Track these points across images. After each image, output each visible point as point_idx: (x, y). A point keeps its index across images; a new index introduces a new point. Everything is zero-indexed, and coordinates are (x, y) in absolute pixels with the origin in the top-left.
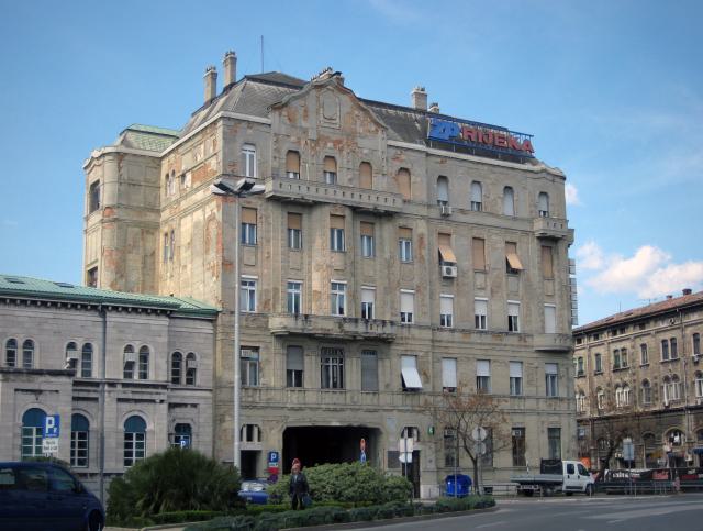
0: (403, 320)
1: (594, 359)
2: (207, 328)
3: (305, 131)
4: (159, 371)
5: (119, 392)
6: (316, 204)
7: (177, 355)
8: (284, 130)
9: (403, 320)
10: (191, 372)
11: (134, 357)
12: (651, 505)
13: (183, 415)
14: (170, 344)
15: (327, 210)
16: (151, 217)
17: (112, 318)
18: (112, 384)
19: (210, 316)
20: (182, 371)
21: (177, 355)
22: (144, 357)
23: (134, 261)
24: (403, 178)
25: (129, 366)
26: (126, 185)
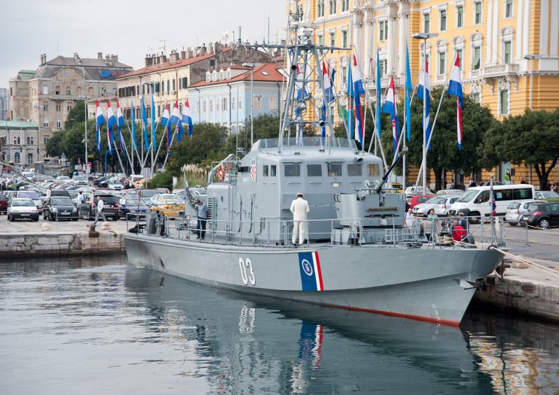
0: (177, 58)
1: (423, 18)
2: (36, 131)
3: (61, 80)
4: (23, 142)
5: (13, 147)
6: (63, 100)
7: (28, 138)
8: (55, 81)
9: (177, 58)
10: (32, 142)
11: (16, 139)
12: (231, 195)
13: (30, 152)
14: (26, 135)
15: (67, 101)
16: (26, 98)
17: (11, 131)
18: (11, 145)
19: (37, 128)
20: (30, 141)
21: (28, 138)
22: (19, 139)
23: (22, 110)
24: (91, 90)
25: (15, 141)
26: (19, 90)
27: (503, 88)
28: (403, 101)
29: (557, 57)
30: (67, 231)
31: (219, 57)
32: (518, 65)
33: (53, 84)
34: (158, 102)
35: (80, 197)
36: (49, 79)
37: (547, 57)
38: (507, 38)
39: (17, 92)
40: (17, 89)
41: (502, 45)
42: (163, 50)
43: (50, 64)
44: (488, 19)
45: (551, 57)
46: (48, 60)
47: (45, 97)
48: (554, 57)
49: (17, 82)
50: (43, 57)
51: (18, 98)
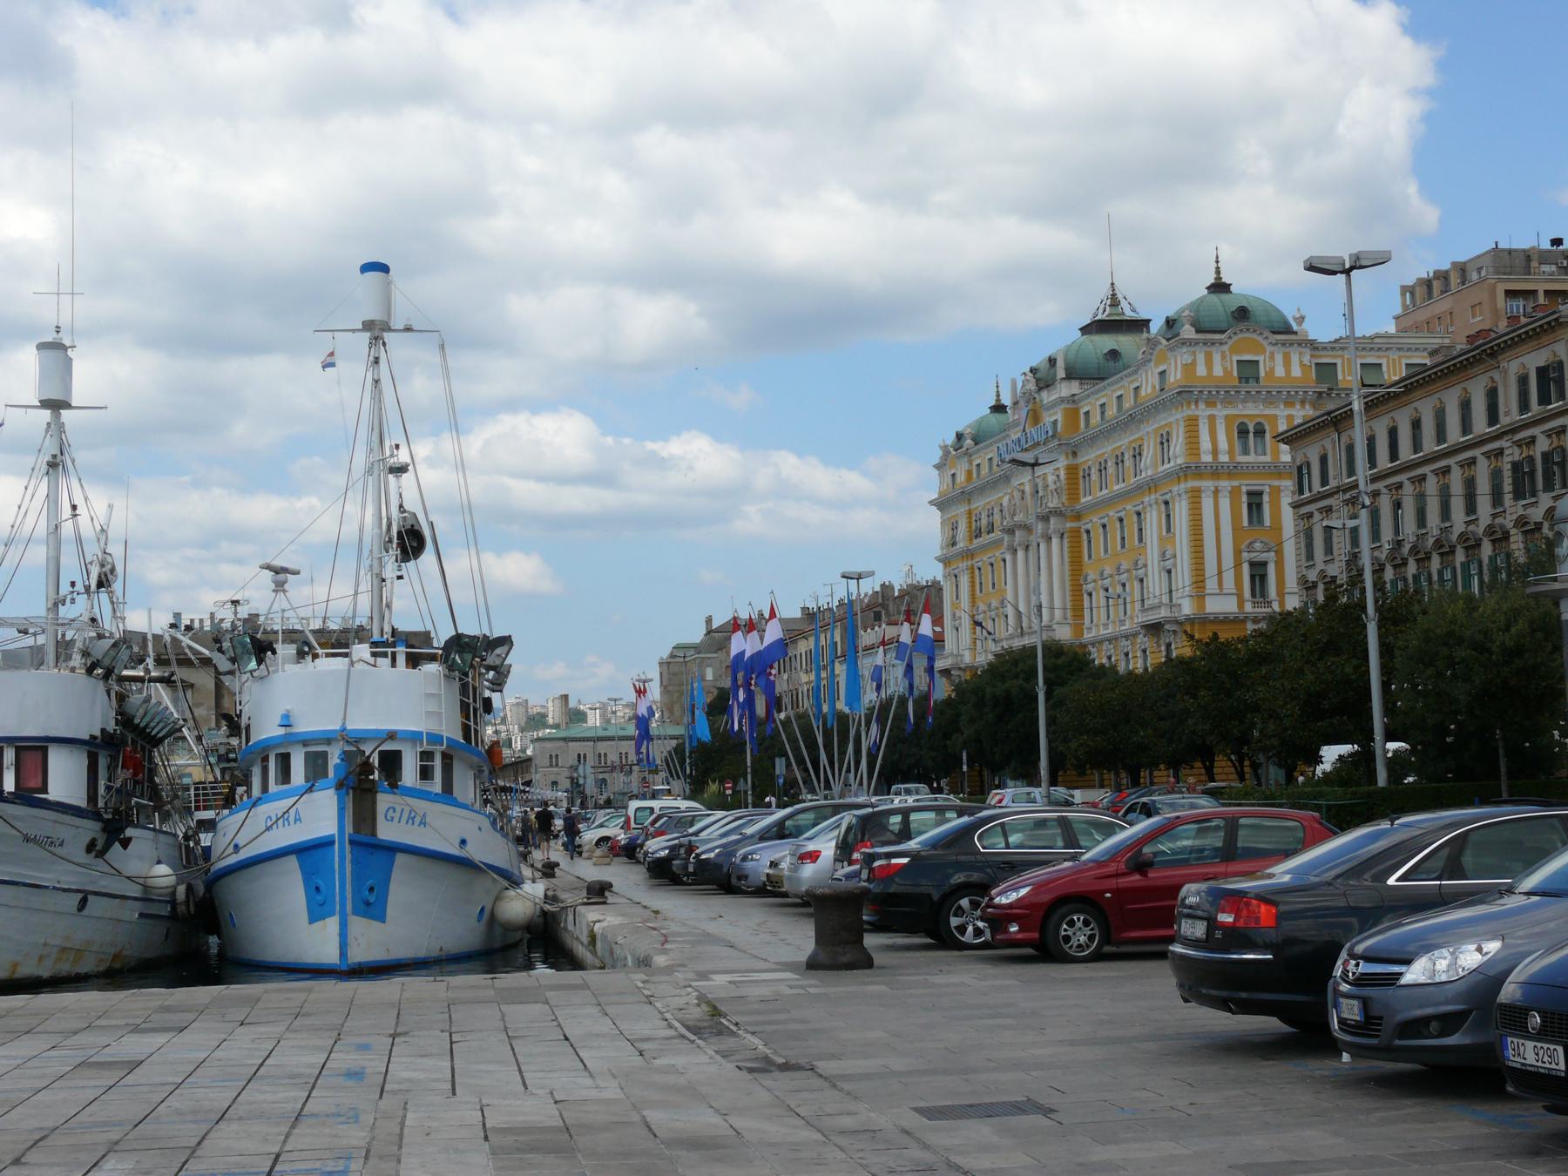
27: (1167, 641)
28: (283, 667)
29: (1234, 591)
30: (1258, 843)
31: (888, 605)
32: (1180, 605)
33: (721, 662)
34: (806, 683)
35: (535, 889)
36: (715, 655)
37: (1218, 591)
38: (1168, 564)
39: (670, 680)
40: (669, 674)
41: (1164, 575)
42: (829, 599)
43: (717, 631)
44: (1294, 557)
45: (1225, 591)
46: (715, 625)
47: (709, 684)
48: (1214, 591)
49: (669, 663)
50: (709, 620)
51: (670, 688)
